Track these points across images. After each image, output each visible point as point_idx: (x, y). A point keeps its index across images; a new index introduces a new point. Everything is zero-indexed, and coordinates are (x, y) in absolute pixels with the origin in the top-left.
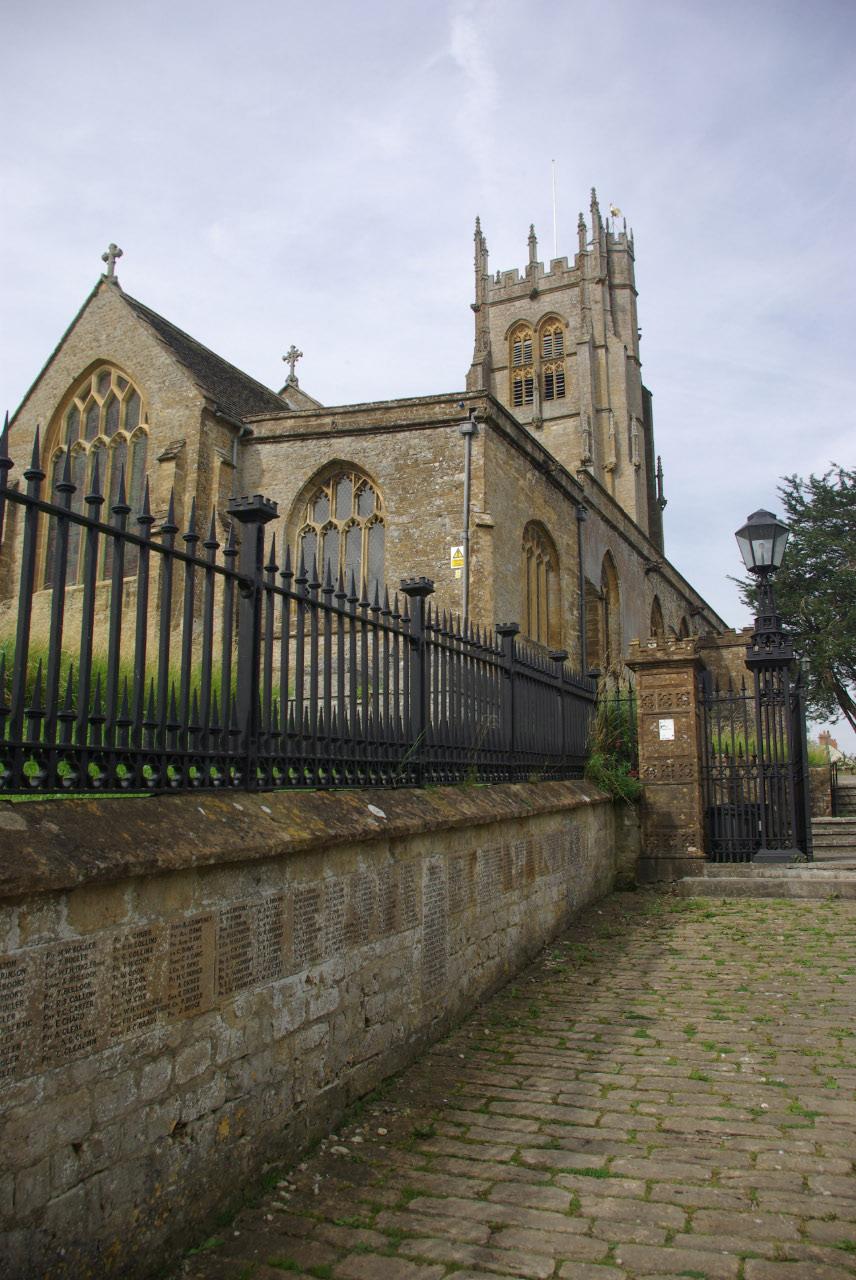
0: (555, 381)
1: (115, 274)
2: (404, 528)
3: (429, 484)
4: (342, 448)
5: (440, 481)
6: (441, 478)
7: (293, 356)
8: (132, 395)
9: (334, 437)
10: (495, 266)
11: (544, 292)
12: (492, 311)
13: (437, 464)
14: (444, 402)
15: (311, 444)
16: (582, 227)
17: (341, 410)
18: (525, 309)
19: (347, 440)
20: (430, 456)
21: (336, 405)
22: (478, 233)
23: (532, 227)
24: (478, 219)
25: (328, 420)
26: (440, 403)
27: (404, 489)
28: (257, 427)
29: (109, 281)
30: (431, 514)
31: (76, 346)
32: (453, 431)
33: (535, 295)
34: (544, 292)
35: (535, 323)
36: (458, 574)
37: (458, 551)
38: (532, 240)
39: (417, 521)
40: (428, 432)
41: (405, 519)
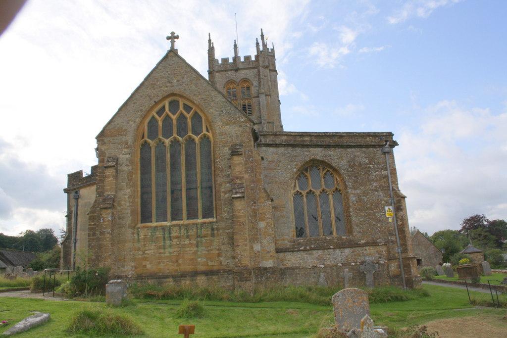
0: (247, 108)
1: (175, 48)
2: (359, 196)
3: (369, 175)
4: (318, 153)
5: (374, 174)
6: (375, 172)
7: (173, 37)
8: (196, 117)
9: (312, 147)
10: (219, 56)
11: (242, 69)
12: (217, 75)
13: (371, 166)
14: (371, 136)
15: (298, 150)
16: (257, 44)
17: (315, 134)
18: (231, 75)
19: (320, 149)
20: (367, 161)
21: (312, 131)
22: (210, 41)
23: (235, 41)
24: (209, 34)
25: (307, 139)
26: (369, 136)
27: (355, 177)
28: (263, 138)
29: (173, 52)
30: (372, 190)
31: (155, 84)
32: (378, 150)
33: (237, 70)
34: (242, 69)
35: (238, 82)
36: (390, 220)
37: (389, 209)
38: (235, 46)
39: (365, 194)
40: (364, 149)
41: (358, 191)
